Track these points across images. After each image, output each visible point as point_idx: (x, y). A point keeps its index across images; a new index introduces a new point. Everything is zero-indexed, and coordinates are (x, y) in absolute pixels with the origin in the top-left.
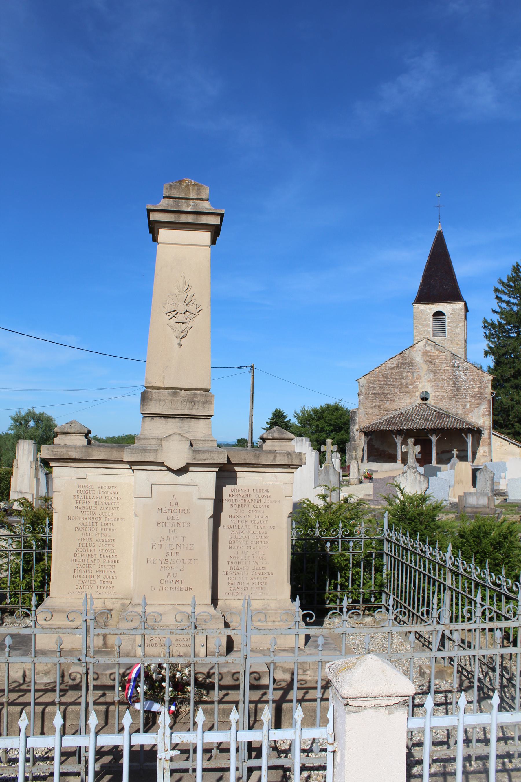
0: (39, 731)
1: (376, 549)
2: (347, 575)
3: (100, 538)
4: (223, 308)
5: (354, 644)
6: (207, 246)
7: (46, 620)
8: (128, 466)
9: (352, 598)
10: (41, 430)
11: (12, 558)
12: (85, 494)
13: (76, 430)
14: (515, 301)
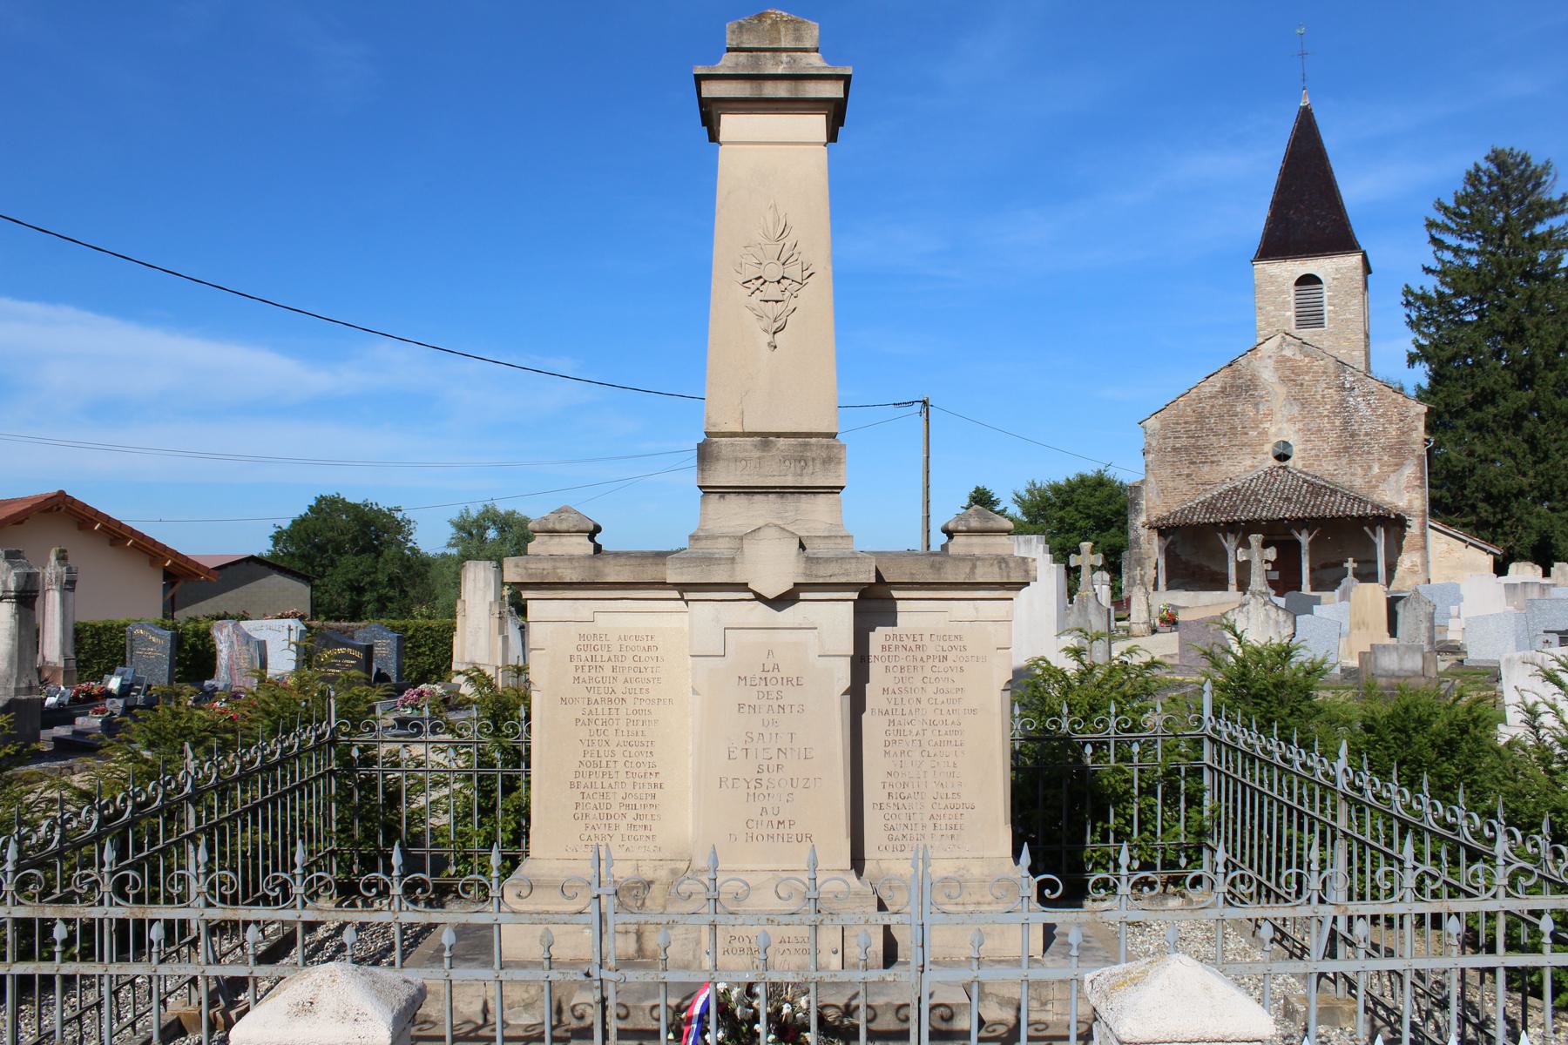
1: (1186, 757)
7: (519, 896)
8: (676, 594)
11: (457, 786)
14: (1473, 246)
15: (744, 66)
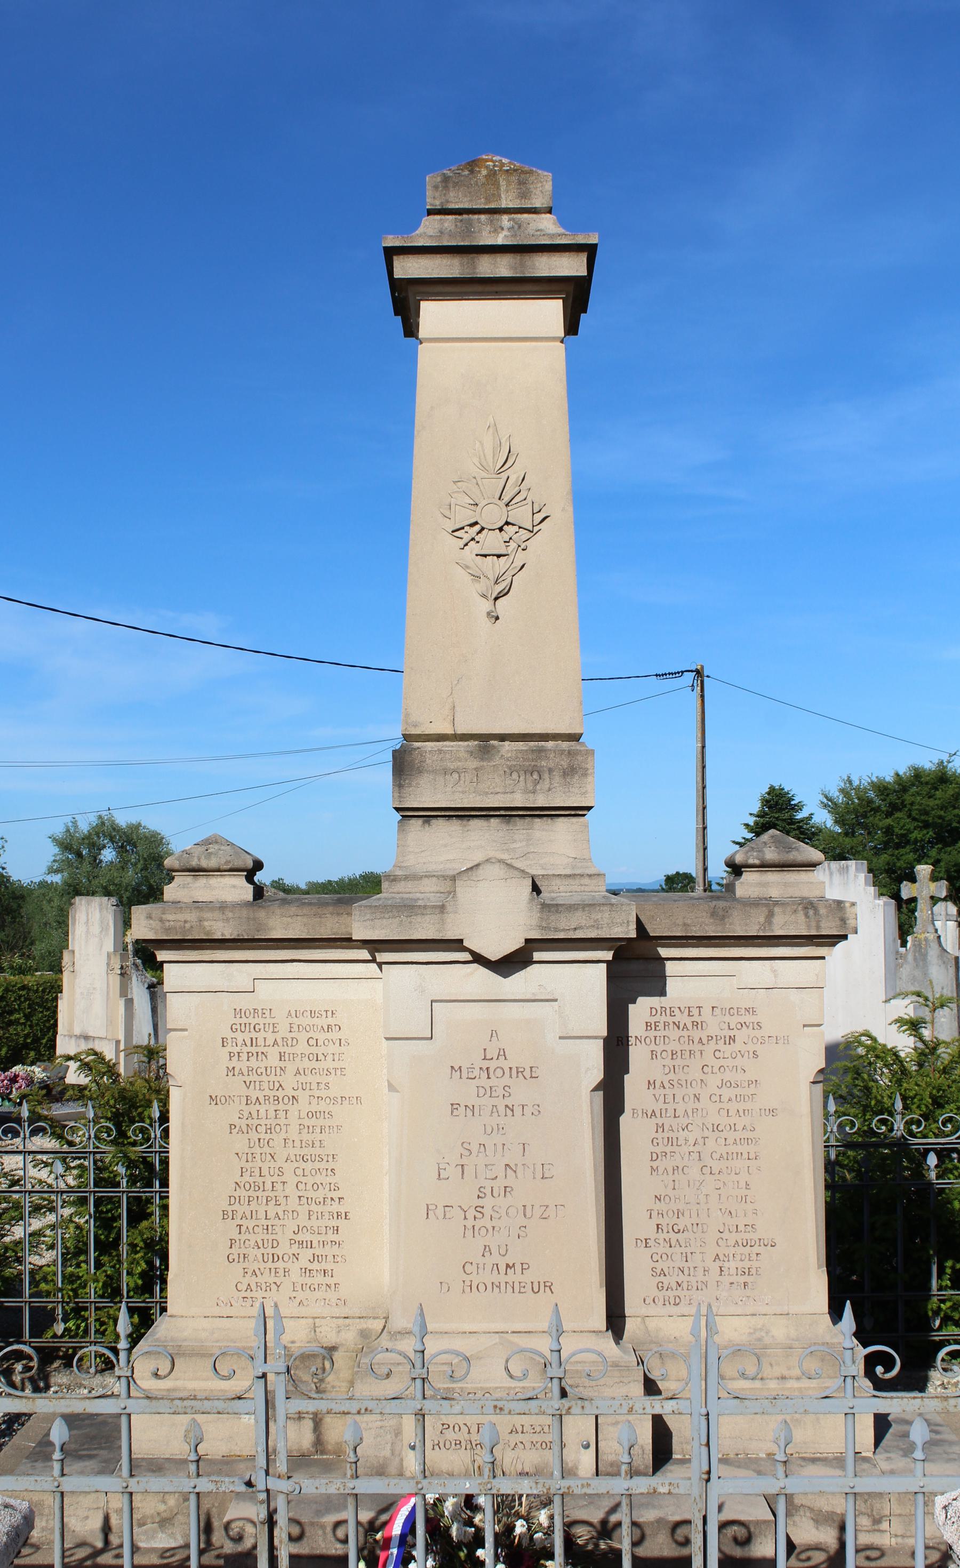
3: (298, 1151)
7: (156, 1375)
8: (364, 954)
10: (129, 867)
11: (67, 1212)
12: (254, 1035)
13: (223, 861)
15: (451, 235)
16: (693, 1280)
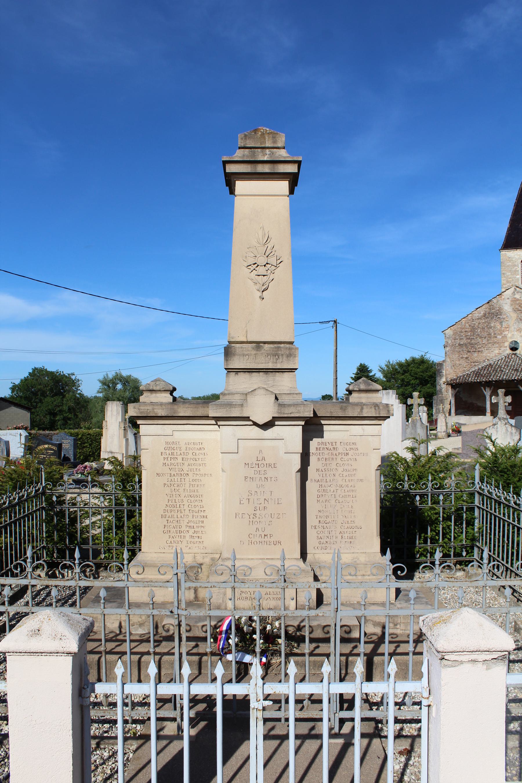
0: (137, 679)
1: (467, 502)
2: (437, 528)
3: (189, 493)
4: (303, 264)
5: (446, 599)
6: (285, 196)
7: (138, 573)
8: (213, 422)
9: (442, 552)
11: (105, 515)
12: (173, 451)
13: (161, 387)
15: (247, 156)
16: (332, 540)
